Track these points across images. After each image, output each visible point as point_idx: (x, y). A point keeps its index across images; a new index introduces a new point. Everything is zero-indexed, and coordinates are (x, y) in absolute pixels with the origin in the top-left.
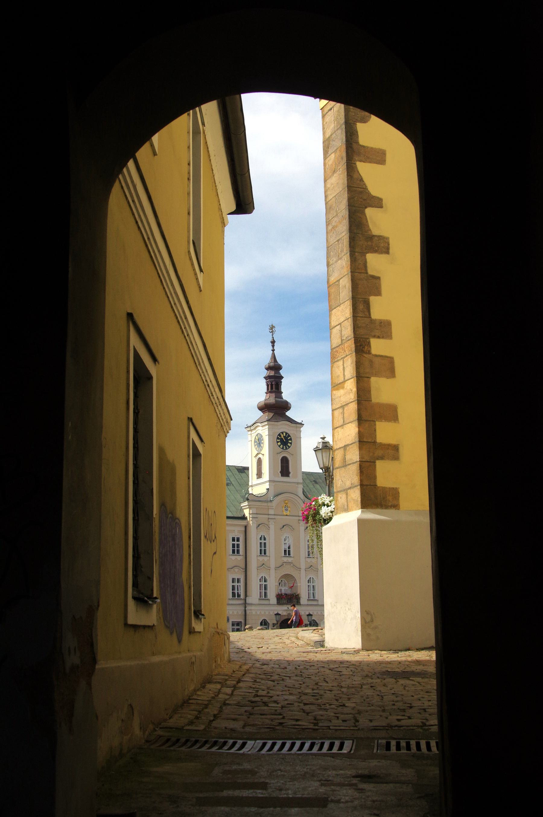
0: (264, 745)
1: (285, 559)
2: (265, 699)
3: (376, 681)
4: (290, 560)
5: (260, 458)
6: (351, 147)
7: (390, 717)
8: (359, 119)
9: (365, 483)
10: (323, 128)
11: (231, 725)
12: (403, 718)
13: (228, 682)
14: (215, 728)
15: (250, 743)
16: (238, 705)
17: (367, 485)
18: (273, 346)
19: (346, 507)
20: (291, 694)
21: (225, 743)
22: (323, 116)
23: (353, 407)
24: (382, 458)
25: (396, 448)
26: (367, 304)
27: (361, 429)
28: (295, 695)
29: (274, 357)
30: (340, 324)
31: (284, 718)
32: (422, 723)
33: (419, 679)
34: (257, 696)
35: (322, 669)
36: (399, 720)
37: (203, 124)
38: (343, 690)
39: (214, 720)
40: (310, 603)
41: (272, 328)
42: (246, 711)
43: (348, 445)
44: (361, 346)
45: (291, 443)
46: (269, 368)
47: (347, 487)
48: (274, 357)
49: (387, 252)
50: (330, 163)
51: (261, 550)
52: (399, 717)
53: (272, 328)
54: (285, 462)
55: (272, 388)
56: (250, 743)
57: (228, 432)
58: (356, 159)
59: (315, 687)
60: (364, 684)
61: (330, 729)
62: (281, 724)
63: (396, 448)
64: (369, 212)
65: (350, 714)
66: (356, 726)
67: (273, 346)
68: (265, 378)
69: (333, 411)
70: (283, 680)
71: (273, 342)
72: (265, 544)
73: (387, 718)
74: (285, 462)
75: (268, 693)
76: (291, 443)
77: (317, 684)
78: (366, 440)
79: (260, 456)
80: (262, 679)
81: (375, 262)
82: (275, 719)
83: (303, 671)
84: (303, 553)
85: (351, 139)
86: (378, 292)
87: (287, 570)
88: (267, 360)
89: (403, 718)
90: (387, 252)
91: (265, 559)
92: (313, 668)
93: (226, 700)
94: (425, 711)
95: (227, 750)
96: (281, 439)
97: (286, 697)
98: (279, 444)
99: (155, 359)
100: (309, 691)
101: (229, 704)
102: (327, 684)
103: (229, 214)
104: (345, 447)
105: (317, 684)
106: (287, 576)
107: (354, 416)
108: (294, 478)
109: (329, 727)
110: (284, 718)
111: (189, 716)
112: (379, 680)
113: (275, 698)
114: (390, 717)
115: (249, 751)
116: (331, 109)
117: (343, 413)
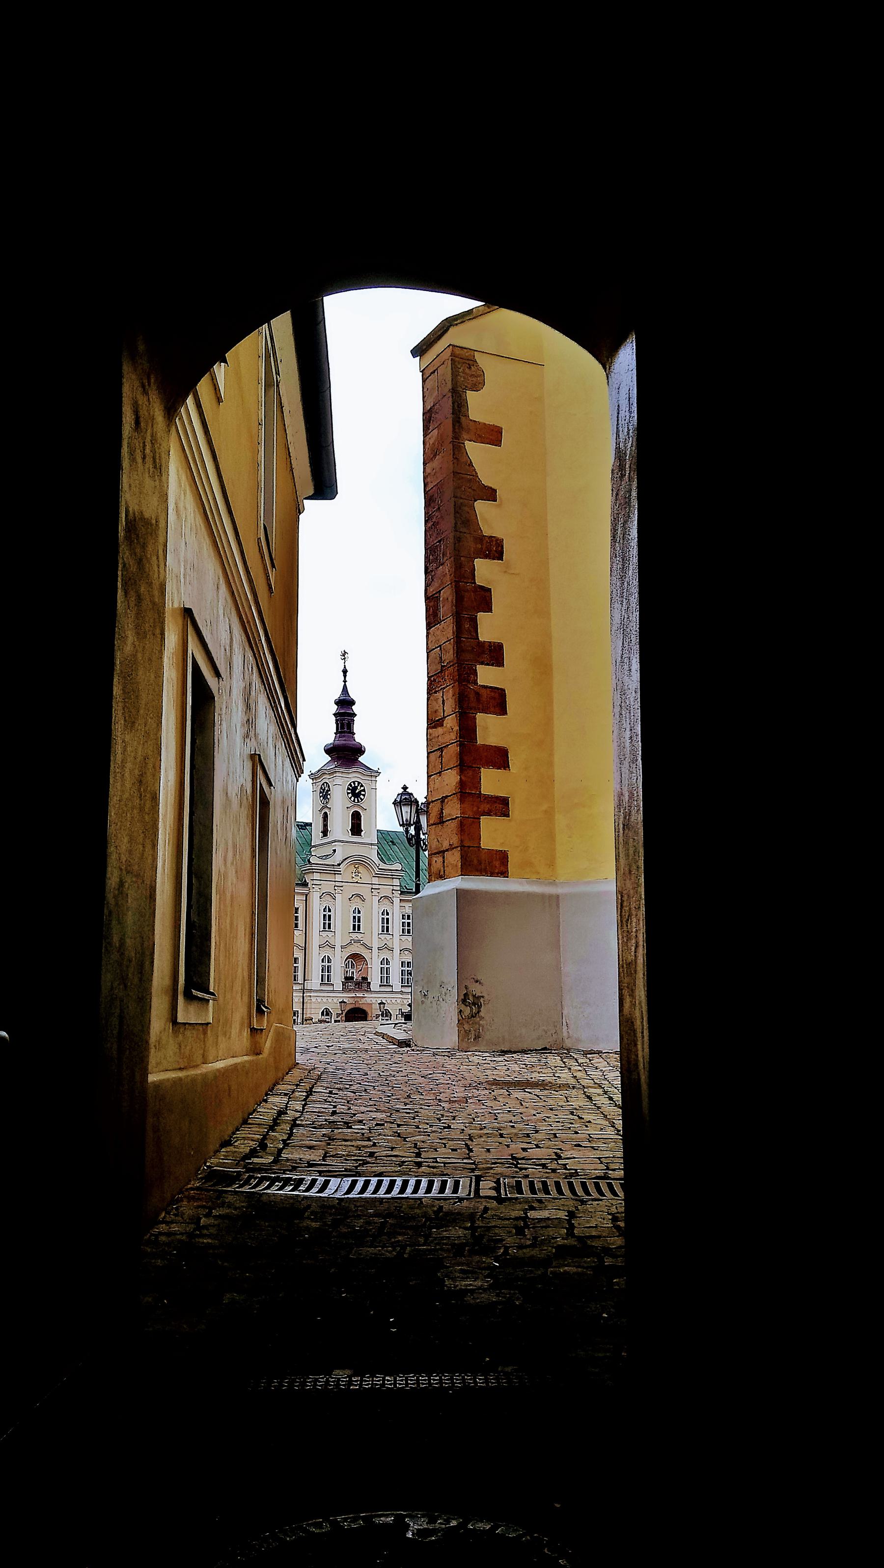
0: (354, 1183)
1: (354, 936)
2: (347, 1118)
3: (483, 1092)
4: (360, 936)
5: (326, 813)
6: (459, 422)
7: (513, 1146)
8: (469, 386)
9: (467, 844)
10: (424, 397)
11: (308, 1156)
12: (530, 1146)
13: (297, 1094)
14: (288, 1160)
15: (334, 1182)
16: (314, 1126)
17: (469, 847)
18: (345, 676)
19: (442, 873)
20: (378, 1111)
21: (300, 1182)
22: (424, 381)
23: (454, 749)
24: (488, 814)
25: (505, 801)
26: (474, 622)
27: (463, 778)
28: (384, 1111)
29: (345, 690)
30: (440, 646)
31: (374, 1145)
32: (556, 1153)
33: (537, 1091)
34: (334, 1113)
35: (413, 1077)
36: (524, 1150)
37: (278, 373)
38: (443, 1104)
39: (284, 1148)
40: (383, 989)
41: (344, 654)
42: (324, 1135)
43: (447, 796)
44: (464, 676)
45: (364, 795)
46: (339, 703)
47: (444, 848)
48: (345, 690)
49: (500, 557)
50: (431, 442)
51: (324, 924)
52: (525, 1146)
53: (344, 654)
54: (356, 817)
55: (342, 727)
56: (334, 1182)
57: (300, 776)
58: (465, 437)
59: (407, 1101)
60: (470, 1098)
61: (437, 1162)
62: (372, 1154)
63: (505, 801)
64: (480, 506)
65: (459, 1140)
66: (469, 1158)
67: (345, 676)
68: (334, 714)
69: (428, 753)
70: (366, 1090)
71: (345, 672)
72: (330, 916)
73: (508, 1146)
74: (356, 817)
75: (349, 1109)
76: (364, 795)
77: (409, 1096)
78: (468, 790)
79: (326, 810)
80: (339, 1089)
81: (484, 571)
82: (364, 1146)
83: (389, 1079)
84: (377, 926)
85: (460, 412)
86: (487, 607)
87: (356, 949)
88: (337, 694)
89: (530, 1146)
90: (500, 557)
91: (330, 934)
92: (400, 1074)
93: (296, 1119)
94: (556, 1137)
95: (304, 1191)
96: (356, 788)
97: (374, 1115)
98: (350, 795)
99: (218, 674)
100: (400, 1106)
101: (299, 1125)
102: (422, 1097)
103: (306, 499)
104: (443, 800)
105: (409, 1096)
106: (356, 957)
107: (454, 762)
108: (369, 835)
109: (436, 1158)
110: (374, 1145)
111: (252, 1143)
112: (487, 1092)
113: (359, 1117)
114: (513, 1146)
115: (336, 1191)
116: (434, 372)
117: (441, 756)
